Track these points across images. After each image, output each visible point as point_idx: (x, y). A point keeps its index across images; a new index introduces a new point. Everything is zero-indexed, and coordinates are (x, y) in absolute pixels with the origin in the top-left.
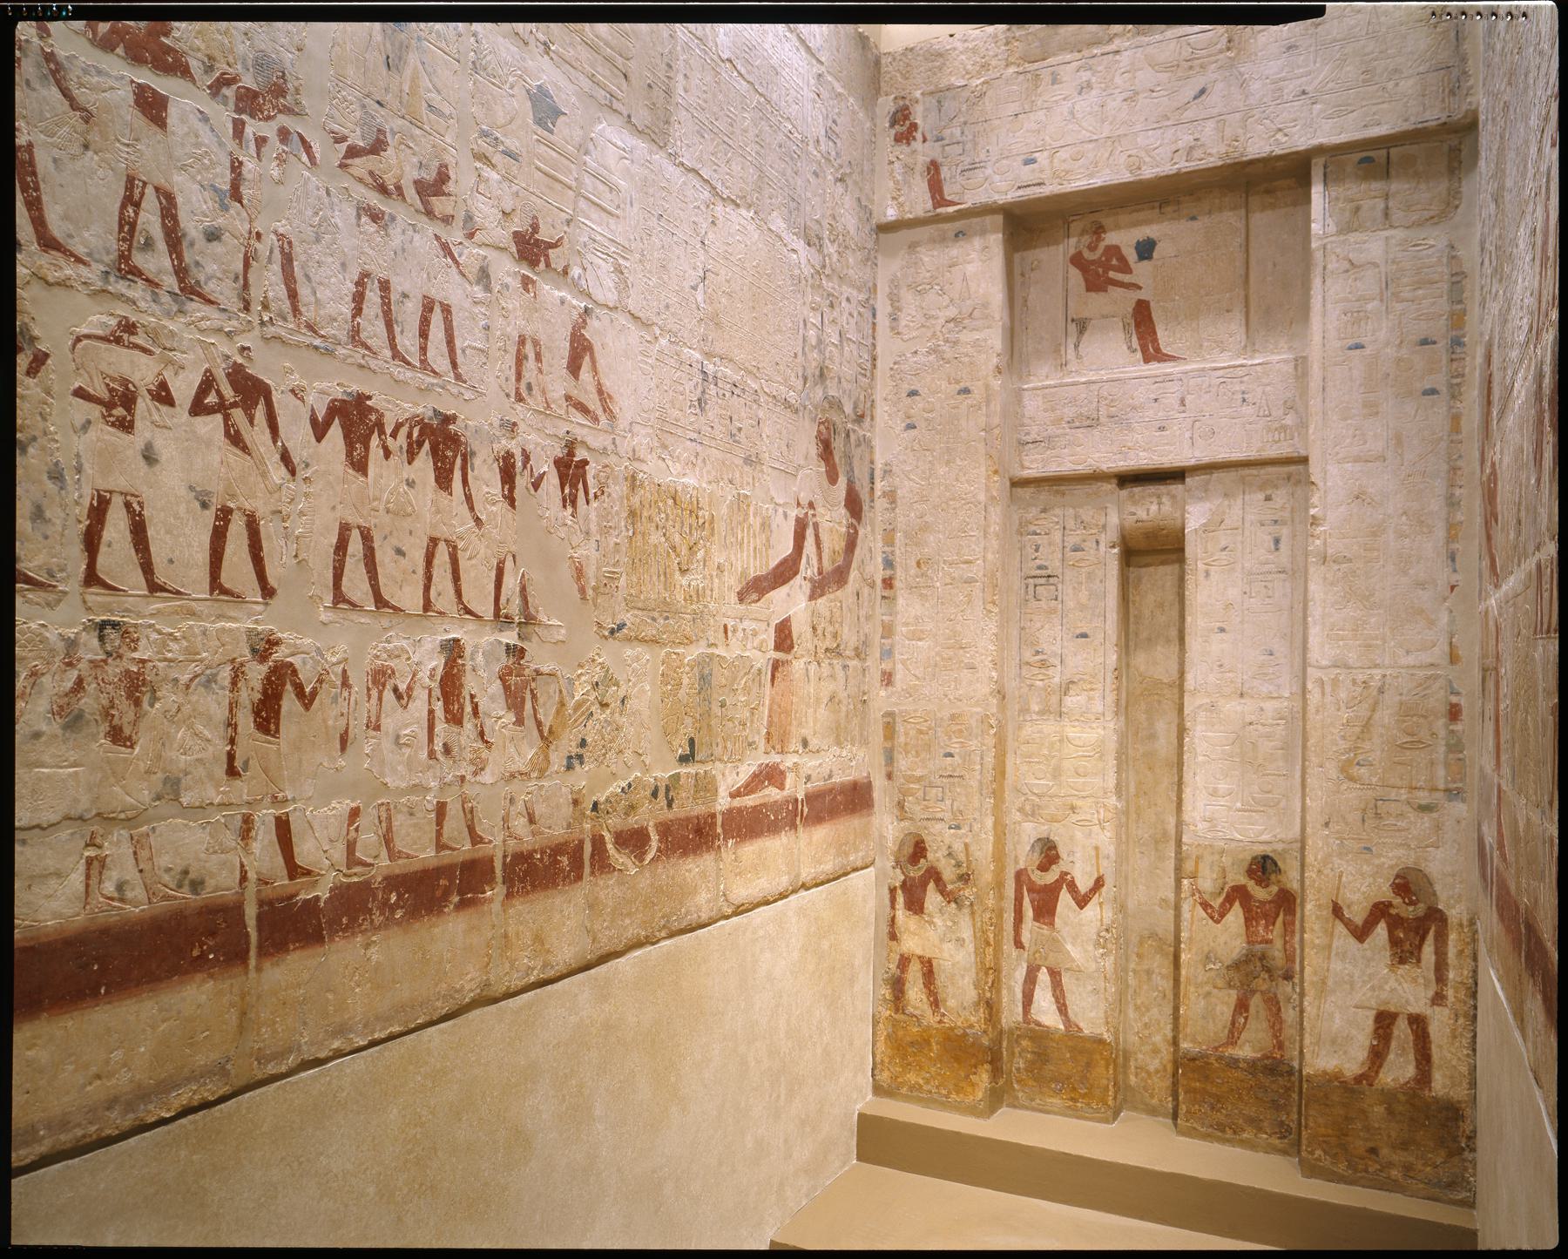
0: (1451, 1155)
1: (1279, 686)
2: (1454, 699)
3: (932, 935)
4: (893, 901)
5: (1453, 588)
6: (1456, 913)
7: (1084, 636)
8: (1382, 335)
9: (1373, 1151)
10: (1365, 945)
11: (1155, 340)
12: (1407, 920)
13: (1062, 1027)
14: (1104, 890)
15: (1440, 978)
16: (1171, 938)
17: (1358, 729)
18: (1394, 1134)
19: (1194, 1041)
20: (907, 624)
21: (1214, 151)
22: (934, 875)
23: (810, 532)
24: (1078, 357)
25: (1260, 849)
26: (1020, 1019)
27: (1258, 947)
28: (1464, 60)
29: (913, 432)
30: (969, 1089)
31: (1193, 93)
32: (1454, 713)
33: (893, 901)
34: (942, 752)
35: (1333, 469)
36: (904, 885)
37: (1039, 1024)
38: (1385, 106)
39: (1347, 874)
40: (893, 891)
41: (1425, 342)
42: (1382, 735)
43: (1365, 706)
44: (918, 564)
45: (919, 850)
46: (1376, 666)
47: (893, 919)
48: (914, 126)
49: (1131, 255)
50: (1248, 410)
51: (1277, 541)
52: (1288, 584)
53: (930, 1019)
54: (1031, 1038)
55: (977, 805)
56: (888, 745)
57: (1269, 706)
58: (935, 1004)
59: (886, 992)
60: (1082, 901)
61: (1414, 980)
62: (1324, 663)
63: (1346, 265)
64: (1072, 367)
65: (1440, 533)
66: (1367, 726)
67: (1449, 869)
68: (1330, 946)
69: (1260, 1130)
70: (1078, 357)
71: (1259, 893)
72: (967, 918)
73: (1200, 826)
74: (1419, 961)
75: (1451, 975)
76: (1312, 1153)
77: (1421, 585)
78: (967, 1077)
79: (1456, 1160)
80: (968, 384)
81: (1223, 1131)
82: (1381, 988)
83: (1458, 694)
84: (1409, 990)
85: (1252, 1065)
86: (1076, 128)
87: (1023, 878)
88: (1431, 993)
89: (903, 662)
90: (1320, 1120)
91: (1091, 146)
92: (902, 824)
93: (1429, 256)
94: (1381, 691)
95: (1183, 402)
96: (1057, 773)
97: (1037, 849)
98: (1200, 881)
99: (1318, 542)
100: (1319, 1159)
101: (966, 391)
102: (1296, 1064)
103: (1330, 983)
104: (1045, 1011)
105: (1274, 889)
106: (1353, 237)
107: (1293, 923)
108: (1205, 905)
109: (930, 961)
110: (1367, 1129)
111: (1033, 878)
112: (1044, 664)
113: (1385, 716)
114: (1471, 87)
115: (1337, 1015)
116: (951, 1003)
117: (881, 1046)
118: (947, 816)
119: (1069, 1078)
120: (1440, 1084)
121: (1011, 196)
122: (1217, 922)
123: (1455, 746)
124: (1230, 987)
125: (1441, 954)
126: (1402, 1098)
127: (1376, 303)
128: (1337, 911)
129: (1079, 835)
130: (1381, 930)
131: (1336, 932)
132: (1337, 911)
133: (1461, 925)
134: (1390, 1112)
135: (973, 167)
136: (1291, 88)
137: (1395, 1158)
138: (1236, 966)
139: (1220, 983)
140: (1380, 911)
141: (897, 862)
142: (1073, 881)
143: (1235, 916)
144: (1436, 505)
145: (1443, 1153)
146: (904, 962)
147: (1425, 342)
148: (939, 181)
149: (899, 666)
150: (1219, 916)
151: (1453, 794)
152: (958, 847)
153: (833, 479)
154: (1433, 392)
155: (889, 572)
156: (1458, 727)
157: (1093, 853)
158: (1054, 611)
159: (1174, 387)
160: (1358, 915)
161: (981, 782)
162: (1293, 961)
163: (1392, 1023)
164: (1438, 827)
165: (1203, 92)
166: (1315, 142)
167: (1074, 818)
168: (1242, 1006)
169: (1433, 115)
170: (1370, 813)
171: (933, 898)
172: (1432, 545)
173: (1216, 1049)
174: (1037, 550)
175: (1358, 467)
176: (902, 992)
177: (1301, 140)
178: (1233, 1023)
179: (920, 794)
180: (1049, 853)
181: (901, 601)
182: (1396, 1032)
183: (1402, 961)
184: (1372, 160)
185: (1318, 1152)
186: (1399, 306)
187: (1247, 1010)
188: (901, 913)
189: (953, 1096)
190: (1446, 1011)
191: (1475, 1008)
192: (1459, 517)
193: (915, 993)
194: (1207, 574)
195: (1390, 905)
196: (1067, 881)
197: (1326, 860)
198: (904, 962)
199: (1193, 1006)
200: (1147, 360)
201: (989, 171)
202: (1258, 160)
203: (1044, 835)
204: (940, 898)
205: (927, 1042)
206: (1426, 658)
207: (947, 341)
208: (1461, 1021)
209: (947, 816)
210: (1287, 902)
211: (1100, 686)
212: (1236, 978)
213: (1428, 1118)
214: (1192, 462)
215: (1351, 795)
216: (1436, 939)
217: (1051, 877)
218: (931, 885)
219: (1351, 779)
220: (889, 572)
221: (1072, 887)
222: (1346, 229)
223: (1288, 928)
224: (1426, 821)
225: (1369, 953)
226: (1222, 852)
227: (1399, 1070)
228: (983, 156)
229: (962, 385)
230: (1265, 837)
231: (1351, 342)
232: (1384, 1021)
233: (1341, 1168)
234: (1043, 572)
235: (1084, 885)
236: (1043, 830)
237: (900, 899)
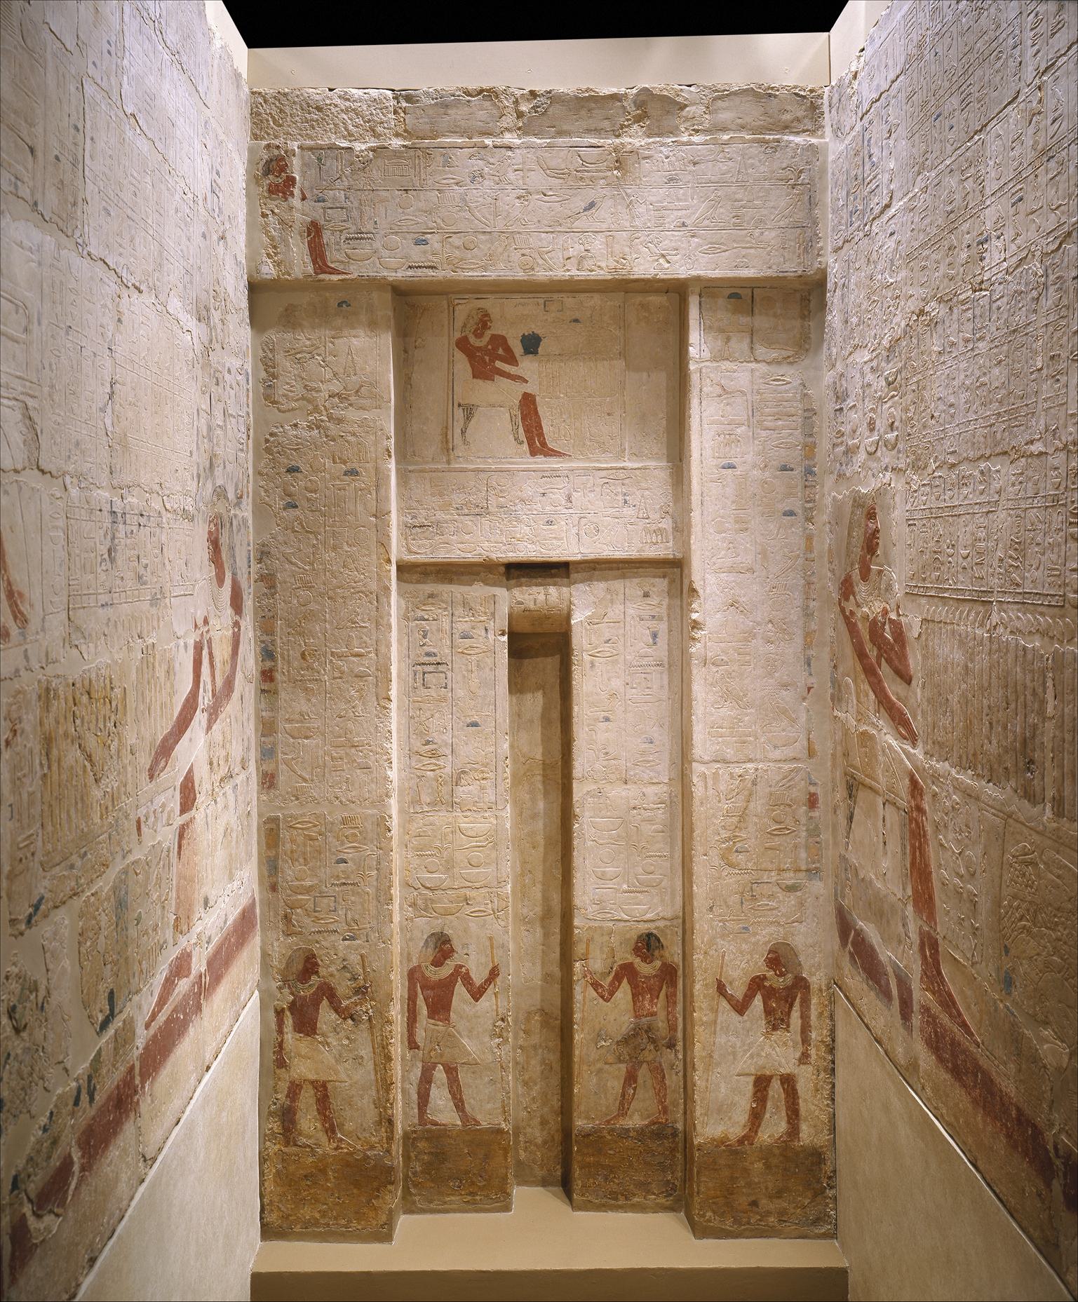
0: (815, 1196)
1: (659, 773)
2: (812, 789)
3: (327, 1056)
4: (280, 1024)
5: (809, 689)
6: (817, 979)
7: (475, 724)
8: (749, 458)
9: (754, 1204)
10: (745, 1017)
11: (541, 435)
12: (778, 991)
13: (459, 1123)
14: (498, 980)
15: (806, 1041)
16: (558, 1012)
17: (735, 820)
18: (770, 1185)
19: (588, 1118)
20: (289, 721)
21: (603, 265)
22: (327, 991)
23: (205, 652)
24: (465, 442)
25: (643, 928)
26: (416, 1121)
27: (644, 1020)
28: (815, 223)
29: (292, 513)
30: (372, 1214)
31: (583, 205)
32: (812, 802)
33: (280, 1024)
34: (334, 858)
35: (711, 579)
36: (292, 1007)
37: (436, 1124)
38: (752, 251)
39: (726, 952)
40: (279, 1013)
41: (784, 468)
42: (756, 824)
43: (741, 797)
44: (303, 655)
45: (309, 966)
46: (750, 761)
47: (281, 1045)
48: (291, 181)
49: (518, 349)
50: (629, 511)
51: (655, 636)
52: (666, 677)
53: (327, 1147)
54: (427, 1139)
55: (373, 912)
56: (272, 853)
57: (651, 790)
58: (331, 1130)
59: (275, 1126)
60: (477, 993)
61: (785, 1044)
62: (706, 758)
63: (719, 391)
64: (458, 452)
65: (799, 640)
66: (743, 817)
67: (810, 941)
68: (715, 1022)
69: (649, 1192)
70: (465, 442)
71: (645, 969)
72: (366, 1034)
73: (590, 909)
74: (788, 1026)
75: (813, 1035)
76: (703, 1216)
77: (785, 686)
78: (369, 1202)
79: (819, 1198)
80: (355, 465)
81: (616, 1199)
82: (759, 1055)
83: (815, 784)
84: (780, 1054)
85: (641, 1132)
86: (468, 215)
87: (417, 975)
88: (798, 1055)
89: (286, 762)
90: (710, 1185)
91: (483, 237)
92: (290, 940)
93: (786, 392)
94: (754, 783)
95: (569, 499)
96: (449, 865)
97: (431, 945)
98: (591, 962)
99: (698, 645)
100: (709, 1221)
101: (353, 473)
102: (680, 1126)
103: (716, 1056)
104: (442, 1109)
105: (658, 963)
106: (726, 365)
107: (675, 995)
108: (596, 985)
109: (324, 1085)
110: (749, 1185)
111: (428, 974)
112: (434, 755)
113: (758, 806)
114: (821, 248)
115: (723, 1085)
116: (349, 1126)
117: (270, 1186)
118: (342, 927)
119: (467, 1172)
120: (806, 1135)
121: (401, 275)
122: (607, 1000)
123: (814, 832)
124: (620, 1061)
125: (805, 1017)
126: (777, 1151)
127: (743, 428)
128: (721, 989)
129: (473, 926)
130: (758, 1002)
131: (721, 1008)
132: (721, 989)
133: (821, 990)
134: (768, 1166)
135: (359, 236)
136: (672, 218)
137: (772, 1207)
138: (626, 1041)
139: (611, 1059)
140: (757, 984)
141: (285, 981)
142: (468, 973)
143: (624, 993)
144: (795, 615)
145: (809, 1194)
146: (295, 1089)
147: (784, 468)
148: (321, 245)
149: (283, 767)
150: (607, 995)
151: (813, 873)
152: (354, 958)
153: (220, 580)
154: (790, 513)
155: (269, 664)
156: (816, 814)
157: (488, 943)
158: (444, 699)
159: (560, 483)
160: (738, 990)
161: (378, 889)
162: (676, 1030)
163: (768, 1086)
164: (801, 904)
165: (592, 205)
166: (694, 273)
167: (468, 910)
168: (631, 1078)
169: (791, 267)
170: (747, 896)
171: (326, 1016)
172: (792, 649)
173: (608, 1122)
174: (424, 637)
175: (731, 577)
176: (293, 1122)
177: (681, 270)
178: (623, 1095)
179: (310, 905)
180: (442, 947)
181: (283, 695)
182: (771, 1093)
183: (775, 1028)
184: (742, 299)
185: (709, 1214)
186: (764, 433)
187: (635, 1082)
188: (290, 1036)
189: (354, 1224)
190: (810, 1069)
191: (833, 1062)
192: (813, 626)
193: (308, 1122)
194: (593, 665)
195: (765, 978)
196: (461, 974)
197: (712, 942)
198: (295, 1089)
199: (585, 1085)
200: (533, 453)
201: (377, 244)
202: (643, 280)
203: (438, 930)
204: (334, 1016)
205: (323, 1171)
206: (789, 752)
207: (330, 418)
208: (822, 1075)
209: (342, 927)
210: (669, 974)
211: (491, 775)
212: (625, 1051)
213: (797, 1166)
214: (579, 557)
215: (731, 880)
216: (801, 1006)
217: (446, 971)
218: (325, 1002)
219: (731, 865)
220: (269, 664)
221: (467, 980)
222: (718, 357)
223: (671, 1000)
224: (792, 899)
225: (748, 1024)
226: (610, 933)
227: (774, 1127)
228: (369, 227)
229: (349, 466)
230: (649, 916)
231: (725, 462)
232: (762, 1084)
233: (728, 1225)
234: (432, 659)
235: (478, 977)
236: (437, 925)
237: (289, 1021)
